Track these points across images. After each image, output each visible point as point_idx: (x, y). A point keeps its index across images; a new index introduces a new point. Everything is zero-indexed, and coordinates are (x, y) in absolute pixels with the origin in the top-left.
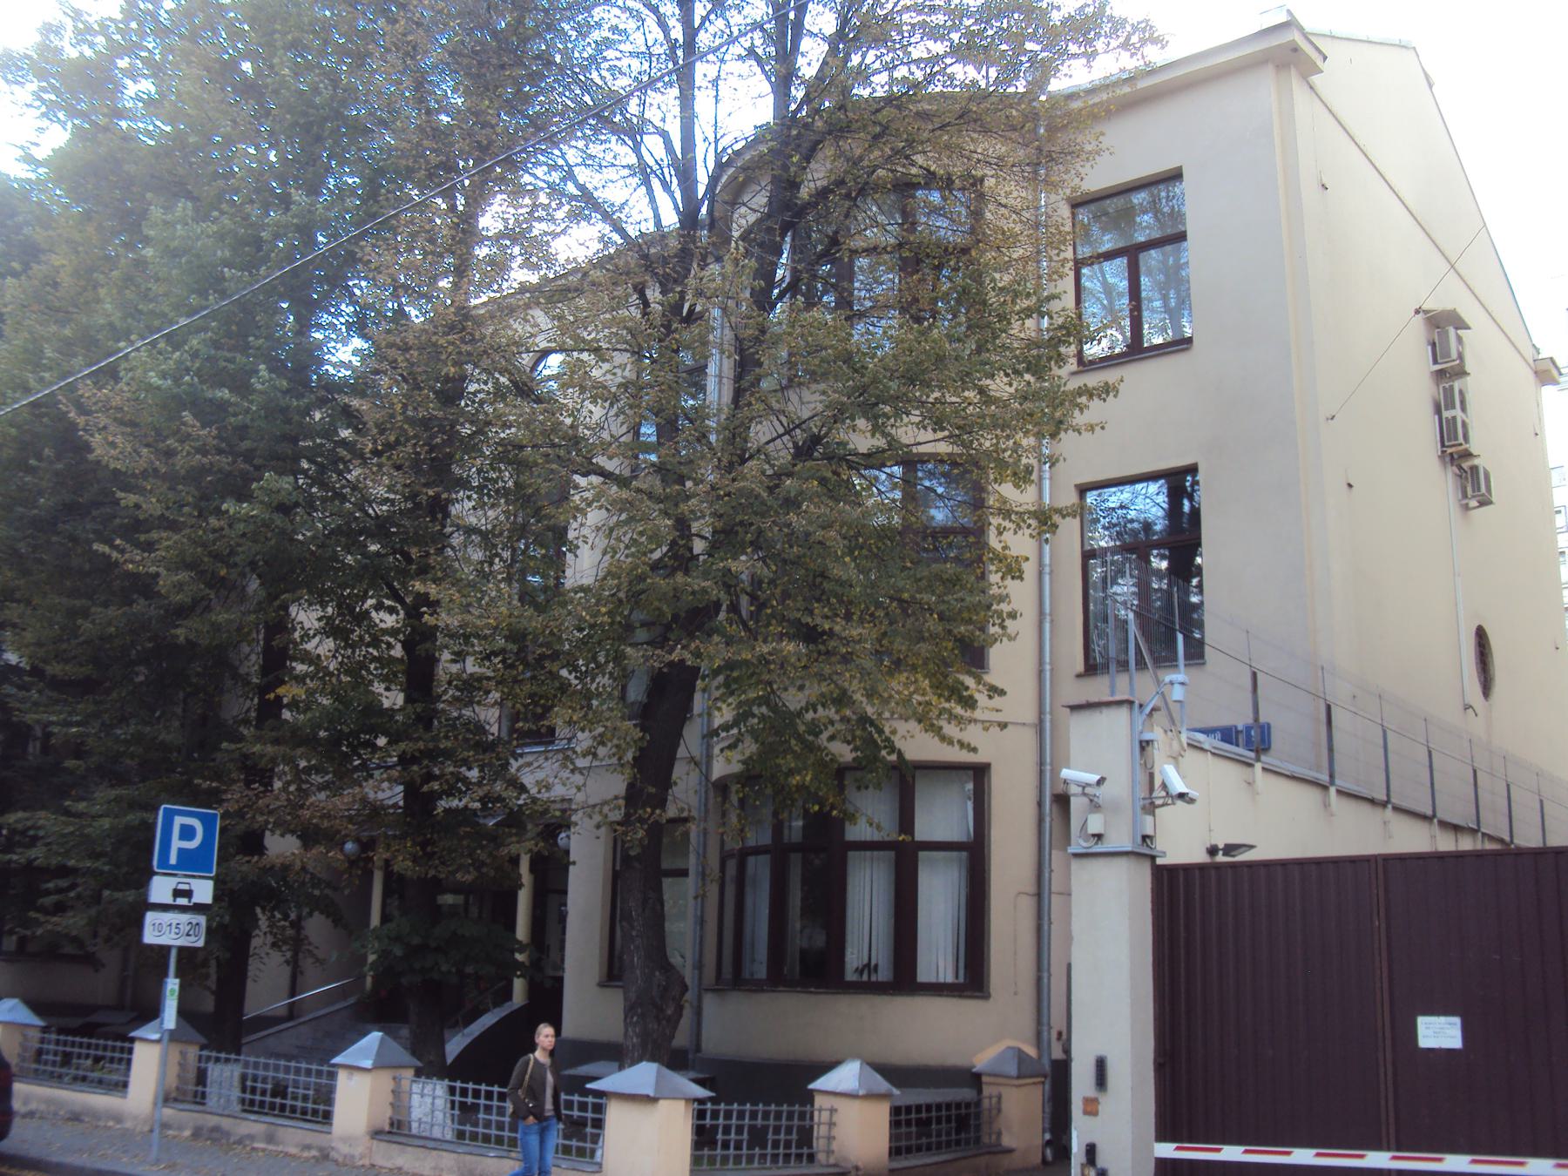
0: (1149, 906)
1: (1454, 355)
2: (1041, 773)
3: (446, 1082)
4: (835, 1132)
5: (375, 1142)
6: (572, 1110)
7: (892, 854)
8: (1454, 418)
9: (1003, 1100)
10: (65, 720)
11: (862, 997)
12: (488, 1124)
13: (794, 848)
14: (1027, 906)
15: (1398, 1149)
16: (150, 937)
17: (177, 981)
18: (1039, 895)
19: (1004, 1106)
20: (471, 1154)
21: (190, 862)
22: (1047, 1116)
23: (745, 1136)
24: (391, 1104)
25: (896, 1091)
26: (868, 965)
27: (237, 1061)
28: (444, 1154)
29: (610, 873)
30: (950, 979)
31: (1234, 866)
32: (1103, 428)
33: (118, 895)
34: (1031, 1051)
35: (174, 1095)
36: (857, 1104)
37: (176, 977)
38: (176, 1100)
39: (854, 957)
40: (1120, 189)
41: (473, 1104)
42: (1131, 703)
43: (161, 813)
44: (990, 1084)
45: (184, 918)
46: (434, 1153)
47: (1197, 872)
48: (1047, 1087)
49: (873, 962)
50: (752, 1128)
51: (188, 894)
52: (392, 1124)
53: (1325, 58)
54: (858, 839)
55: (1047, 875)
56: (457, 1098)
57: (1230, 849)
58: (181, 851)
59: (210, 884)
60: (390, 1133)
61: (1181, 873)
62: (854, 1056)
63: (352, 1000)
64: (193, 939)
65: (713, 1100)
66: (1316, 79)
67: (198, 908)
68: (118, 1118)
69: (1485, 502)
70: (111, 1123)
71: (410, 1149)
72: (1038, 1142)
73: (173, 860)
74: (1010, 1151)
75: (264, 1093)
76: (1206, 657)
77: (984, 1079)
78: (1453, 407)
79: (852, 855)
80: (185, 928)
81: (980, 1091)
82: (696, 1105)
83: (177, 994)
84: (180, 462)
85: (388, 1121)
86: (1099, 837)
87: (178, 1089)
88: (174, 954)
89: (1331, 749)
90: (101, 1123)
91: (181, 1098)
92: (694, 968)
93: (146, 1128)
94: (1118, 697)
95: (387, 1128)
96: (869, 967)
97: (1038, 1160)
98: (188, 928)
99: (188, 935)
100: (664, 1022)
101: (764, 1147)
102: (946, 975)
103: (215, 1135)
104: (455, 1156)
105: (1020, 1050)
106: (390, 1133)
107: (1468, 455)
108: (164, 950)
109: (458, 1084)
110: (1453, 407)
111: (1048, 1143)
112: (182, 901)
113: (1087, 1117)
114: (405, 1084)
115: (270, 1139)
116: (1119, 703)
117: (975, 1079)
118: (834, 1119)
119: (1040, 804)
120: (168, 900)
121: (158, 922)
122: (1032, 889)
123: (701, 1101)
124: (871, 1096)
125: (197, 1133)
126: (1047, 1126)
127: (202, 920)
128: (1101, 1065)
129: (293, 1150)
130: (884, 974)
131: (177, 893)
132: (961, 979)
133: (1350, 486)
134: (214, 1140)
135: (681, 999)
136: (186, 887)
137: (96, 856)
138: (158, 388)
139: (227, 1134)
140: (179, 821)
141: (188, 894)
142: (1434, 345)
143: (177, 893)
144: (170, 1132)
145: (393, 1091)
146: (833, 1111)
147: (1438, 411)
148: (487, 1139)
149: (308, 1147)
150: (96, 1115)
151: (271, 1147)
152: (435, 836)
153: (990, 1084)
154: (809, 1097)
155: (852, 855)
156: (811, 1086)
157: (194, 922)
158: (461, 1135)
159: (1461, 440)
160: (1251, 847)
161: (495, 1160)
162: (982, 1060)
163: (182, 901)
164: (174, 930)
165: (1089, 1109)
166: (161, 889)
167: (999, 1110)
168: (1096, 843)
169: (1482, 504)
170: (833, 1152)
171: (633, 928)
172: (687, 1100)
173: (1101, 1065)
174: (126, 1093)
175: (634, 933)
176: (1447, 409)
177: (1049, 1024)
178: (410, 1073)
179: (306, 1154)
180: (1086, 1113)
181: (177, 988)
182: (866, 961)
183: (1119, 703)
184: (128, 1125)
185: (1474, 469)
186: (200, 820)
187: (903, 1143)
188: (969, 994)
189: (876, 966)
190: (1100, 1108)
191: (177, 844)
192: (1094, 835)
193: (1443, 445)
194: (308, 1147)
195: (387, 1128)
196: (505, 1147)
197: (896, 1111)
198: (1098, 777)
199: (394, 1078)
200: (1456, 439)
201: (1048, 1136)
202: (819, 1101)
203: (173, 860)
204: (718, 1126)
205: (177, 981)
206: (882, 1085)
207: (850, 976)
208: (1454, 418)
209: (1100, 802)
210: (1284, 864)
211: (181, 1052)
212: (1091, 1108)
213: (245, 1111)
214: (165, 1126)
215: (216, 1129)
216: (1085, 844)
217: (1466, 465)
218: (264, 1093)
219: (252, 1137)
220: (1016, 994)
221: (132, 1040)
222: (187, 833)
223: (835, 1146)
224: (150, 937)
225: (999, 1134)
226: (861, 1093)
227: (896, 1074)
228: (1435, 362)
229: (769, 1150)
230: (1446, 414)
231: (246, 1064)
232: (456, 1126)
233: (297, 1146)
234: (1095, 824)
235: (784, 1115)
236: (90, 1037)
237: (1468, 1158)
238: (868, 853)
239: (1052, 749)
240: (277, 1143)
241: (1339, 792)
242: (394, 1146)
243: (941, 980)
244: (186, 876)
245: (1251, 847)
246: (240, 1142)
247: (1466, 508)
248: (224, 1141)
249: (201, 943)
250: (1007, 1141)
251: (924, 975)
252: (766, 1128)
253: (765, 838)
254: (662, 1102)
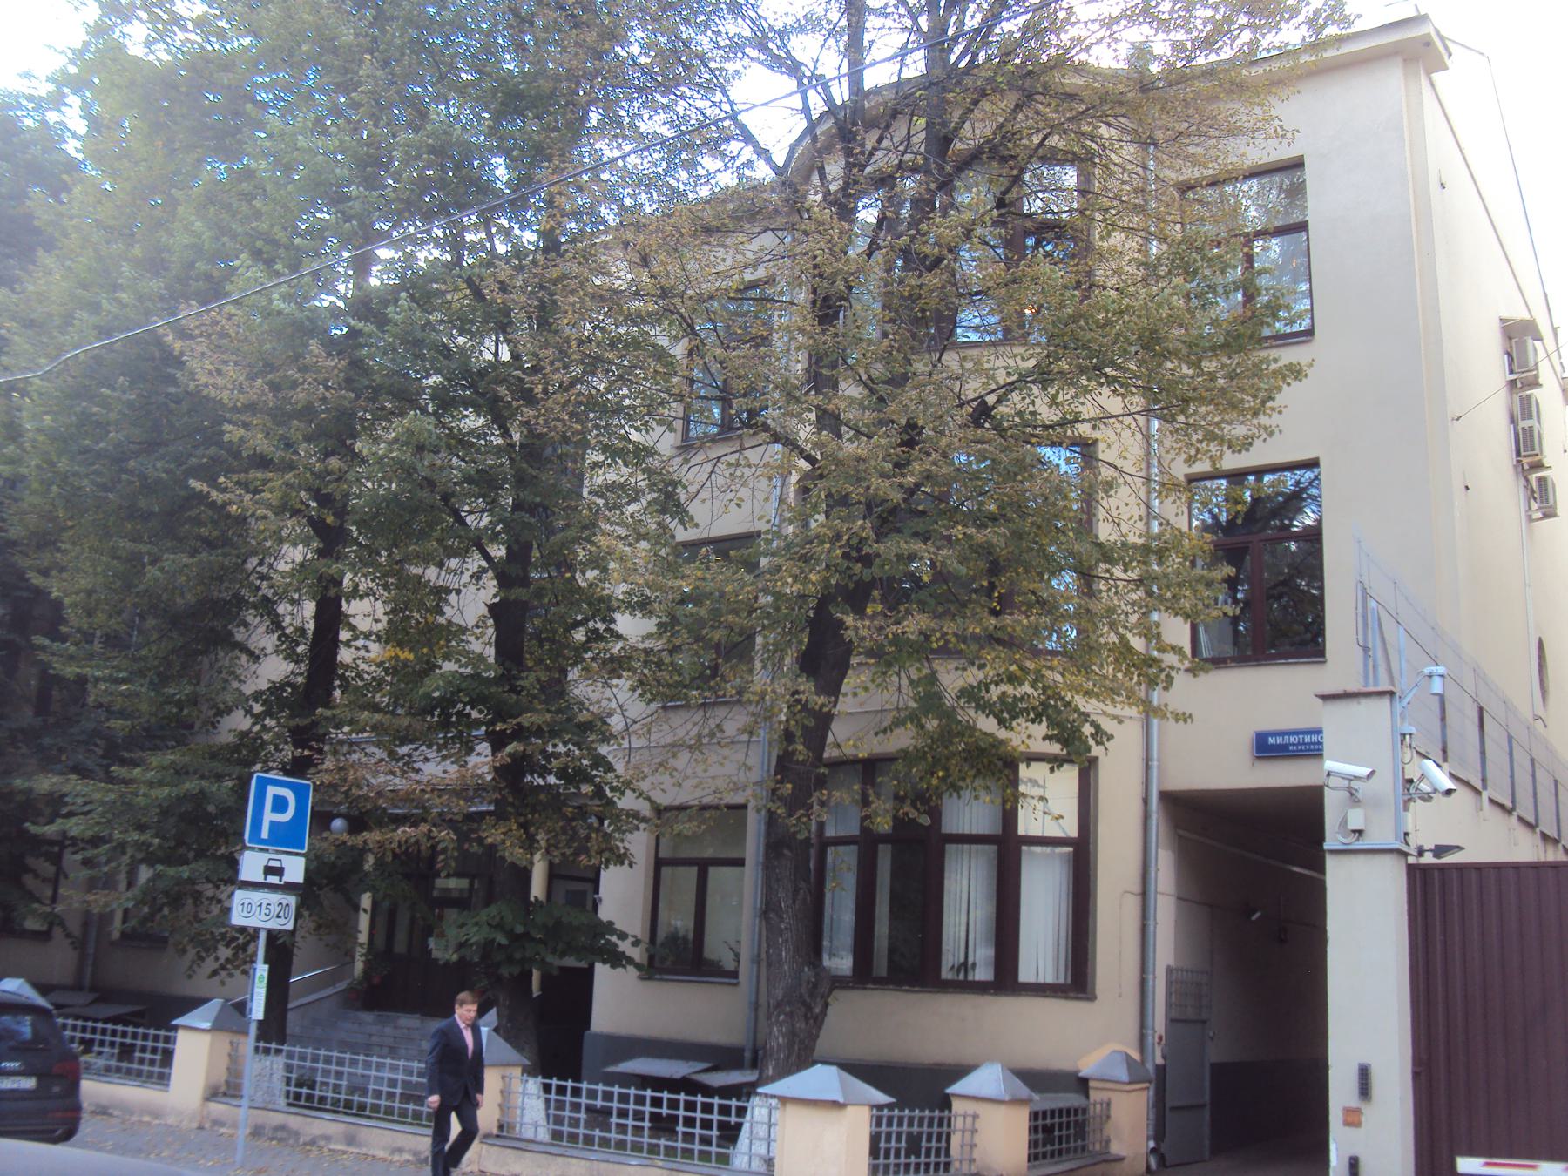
0: (1405, 907)
1: (1532, 364)
2: (1147, 768)
3: (540, 1079)
4: (977, 1139)
5: (485, 1146)
6: (661, 1107)
7: (994, 848)
8: (1531, 428)
9: (1113, 1107)
10: (111, 675)
11: (966, 996)
12: (688, 1137)
13: (884, 838)
14: (1132, 905)
15: (1491, 1155)
16: (238, 918)
17: (267, 967)
18: (1144, 894)
19: (1113, 1113)
20: (608, 1161)
21: (283, 837)
22: (1152, 1122)
23: (903, 1144)
24: (500, 1105)
25: (1036, 1097)
26: (965, 964)
27: (278, 1052)
28: (574, 1161)
29: (652, 861)
30: (1050, 979)
31: (1443, 869)
32: (1280, 412)
33: (171, 871)
34: (1136, 1055)
35: (223, 1089)
36: (1002, 1109)
37: (265, 962)
38: (225, 1094)
39: (951, 955)
40: (1280, 165)
41: (669, 1116)
42: (1392, 694)
43: (254, 782)
44: (1097, 1089)
45: (275, 898)
46: (560, 1159)
47: (1436, 874)
48: (1152, 1093)
49: (970, 960)
50: (909, 1135)
51: (279, 871)
52: (501, 1127)
53: (1450, 55)
54: (955, 831)
55: (1153, 875)
56: (553, 1096)
57: (1440, 851)
58: (273, 824)
59: (301, 862)
60: (498, 1136)
61: (1436, 874)
62: (991, 1059)
63: (342, 986)
64: (283, 921)
65: (890, 1106)
66: (1436, 76)
67: (289, 888)
68: (156, 1114)
69: (1549, 514)
70: (146, 1119)
71: (528, 1155)
72: (1144, 1150)
73: (265, 834)
74: (1121, 1159)
75: (391, 1096)
76: (1327, 655)
77: (1091, 1084)
78: (1530, 417)
79: (951, 849)
80: (275, 909)
81: (1087, 1097)
82: (875, 1111)
83: (265, 981)
84: (299, 397)
85: (495, 1124)
86: (1359, 833)
87: (227, 1082)
88: (263, 936)
89: (1483, 753)
90: (134, 1118)
91: (232, 1092)
92: (753, 962)
93: (195, 1125)
94: (1380, 689)
95: (495, 1131)
96: (965, 966)
97: (1143, 1168)
98: (278, 909)
99: (278, 917)
100: (811, 1021)
101: (918, 1156)
102: (1048, 976)
103: (279, 1134)
104: (588, 1164)
105: (1127, 1055)
106: (498, 1136)
107: (1539, 466)
108: (251, 934)
109: (554, 1082)
110: (1530, 417)
111: (1153, 1151)
112: (273, 880)
113: (1347, 1128)
114: (517, 1086)
115: (351, 1140)
116: (1381, 694)
117: (1082, 1084)
118: (977, 1126)
119: (1146, 801)
120: (260, 878)
121: (247, 902)
122: (1137, 888)
123: (880, 1107)
124: (1016, 1102)
125: (257, 1132)
126: (1151, 1133)
127: (292, 900)
128: (1364, 1074)
129: (381, 1154)
130: (983, 973)
131: (269, 871)
132: (1069, 981)
133: (1467, 488)
134: (280, 1140)
135: (828, 996)
136: (277, 864)
137: (141, 828)
138: (280, 313)
139: (297, 1134)
140: (272, 790)
141: (279, 871)
142: (1510, 355)
143: (269, 871)
144: (222, 1130)
145: (502, 1092)
146: (975, 1117)
147: (1513, 420)
148: (621, 1145)
149: (400, 1150)
150: (127, 1109)
151: (351, 1149)
152: (537, 816)
153: (1097, 1089)
154: (946, 1103)
155: (951, 849)
156: (949, 1090)
157: (284, 903)
158: (557, 1135)
159: (1537, 451)
160: (1459, 848)
161: (639, 1168)
162: (1087, 1066)
163: (273, 880)
164: (264, 911)
165: (1350, 1119)
166: (252, 865)
167: (1108, 1117)
168: (1358, 840)
169: (1546, 516)
170: (974, 1160)
171: (782, 919)
172: (872, 1107)
173: (1364, 1074)
174: (168, 1085)
175: (783, 926)
176: (1523, 419)
177: (1153, 1029)
178: (517, 1071)
179: (396, 1158)
180: (1347, 1123)
181: (266, 974)
182: (962, 959)
183: (1381, 694)
184: (171, 1120)
185: (1542, 482)
186: (295, 792)
187: (1040, 1150)
188: (1072, 995)
189: (974, 965)
190: (1363, 1119)
191: (269, 816)
192: (1354, 831)
193: (1518, 453)
194: (400, 1150)
195: (495, 1131)
196: (645, 1155)
197: (1035, 1116)
198: (1369, 770)
199: (503, 1077)
200: (1533, 450)
201: (1152, 1144)
202: (957, 1106)
203: (265, 834)
204: (719, 1122)
205: (267, 967)
206: (1024, 1091)
207: (946, 974)
208: (1531, 428)
209: (1360, 795)
210: (1478, 868)
211: (231, 1043)
212: (1353, 1118)
213: (289, 1105)
214: (217, 1123)
215: (282, 1128)
216: (1344, 841)
217: (1534, 477)
218: (391, 1096)
219: (328, 1138)
220: (1120, 996)
221: (176, 1028)
222: (281, 803)
223: (976, 1155)
224: (238, 918)
225: (1108, 1142)
226: (1007, 1098)
227: (1036, 1079)
228: (1511, 372)
229: (923, 1159)
230: (1523, 424)
231: (290, 1055)
232: (552, 1126)
233: (384, 1149)
234: (1356, 819)
235: (936, 1121)
236: (158, 1028)
237: (1481, 1161)
238: (966, 847)
239: (1159, 744)
240: (360, 1145)
241: (1491, 801)
242: (509, 1151)
243: (1041, 980)
244: (278, 852)
245: (1459, 848)
246: (313, 1142)
247: (1530, 519)
248: (291, 1141)
249: (290, 927)
250: (1116, 1148)
251: (1026, 974)
252: (920, 1134)
253: (853, 829)
254: (850, 1109)
